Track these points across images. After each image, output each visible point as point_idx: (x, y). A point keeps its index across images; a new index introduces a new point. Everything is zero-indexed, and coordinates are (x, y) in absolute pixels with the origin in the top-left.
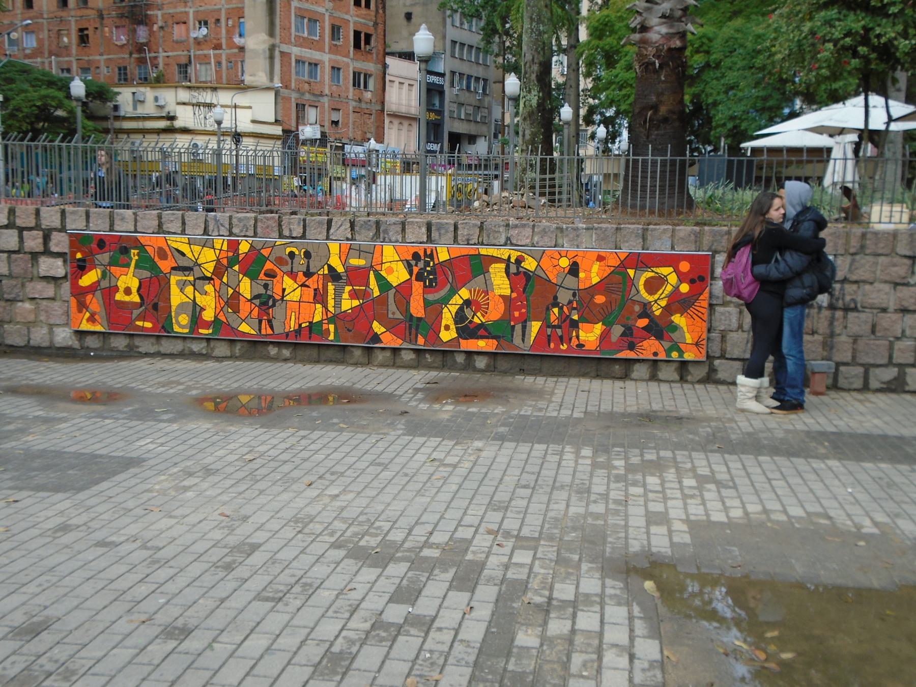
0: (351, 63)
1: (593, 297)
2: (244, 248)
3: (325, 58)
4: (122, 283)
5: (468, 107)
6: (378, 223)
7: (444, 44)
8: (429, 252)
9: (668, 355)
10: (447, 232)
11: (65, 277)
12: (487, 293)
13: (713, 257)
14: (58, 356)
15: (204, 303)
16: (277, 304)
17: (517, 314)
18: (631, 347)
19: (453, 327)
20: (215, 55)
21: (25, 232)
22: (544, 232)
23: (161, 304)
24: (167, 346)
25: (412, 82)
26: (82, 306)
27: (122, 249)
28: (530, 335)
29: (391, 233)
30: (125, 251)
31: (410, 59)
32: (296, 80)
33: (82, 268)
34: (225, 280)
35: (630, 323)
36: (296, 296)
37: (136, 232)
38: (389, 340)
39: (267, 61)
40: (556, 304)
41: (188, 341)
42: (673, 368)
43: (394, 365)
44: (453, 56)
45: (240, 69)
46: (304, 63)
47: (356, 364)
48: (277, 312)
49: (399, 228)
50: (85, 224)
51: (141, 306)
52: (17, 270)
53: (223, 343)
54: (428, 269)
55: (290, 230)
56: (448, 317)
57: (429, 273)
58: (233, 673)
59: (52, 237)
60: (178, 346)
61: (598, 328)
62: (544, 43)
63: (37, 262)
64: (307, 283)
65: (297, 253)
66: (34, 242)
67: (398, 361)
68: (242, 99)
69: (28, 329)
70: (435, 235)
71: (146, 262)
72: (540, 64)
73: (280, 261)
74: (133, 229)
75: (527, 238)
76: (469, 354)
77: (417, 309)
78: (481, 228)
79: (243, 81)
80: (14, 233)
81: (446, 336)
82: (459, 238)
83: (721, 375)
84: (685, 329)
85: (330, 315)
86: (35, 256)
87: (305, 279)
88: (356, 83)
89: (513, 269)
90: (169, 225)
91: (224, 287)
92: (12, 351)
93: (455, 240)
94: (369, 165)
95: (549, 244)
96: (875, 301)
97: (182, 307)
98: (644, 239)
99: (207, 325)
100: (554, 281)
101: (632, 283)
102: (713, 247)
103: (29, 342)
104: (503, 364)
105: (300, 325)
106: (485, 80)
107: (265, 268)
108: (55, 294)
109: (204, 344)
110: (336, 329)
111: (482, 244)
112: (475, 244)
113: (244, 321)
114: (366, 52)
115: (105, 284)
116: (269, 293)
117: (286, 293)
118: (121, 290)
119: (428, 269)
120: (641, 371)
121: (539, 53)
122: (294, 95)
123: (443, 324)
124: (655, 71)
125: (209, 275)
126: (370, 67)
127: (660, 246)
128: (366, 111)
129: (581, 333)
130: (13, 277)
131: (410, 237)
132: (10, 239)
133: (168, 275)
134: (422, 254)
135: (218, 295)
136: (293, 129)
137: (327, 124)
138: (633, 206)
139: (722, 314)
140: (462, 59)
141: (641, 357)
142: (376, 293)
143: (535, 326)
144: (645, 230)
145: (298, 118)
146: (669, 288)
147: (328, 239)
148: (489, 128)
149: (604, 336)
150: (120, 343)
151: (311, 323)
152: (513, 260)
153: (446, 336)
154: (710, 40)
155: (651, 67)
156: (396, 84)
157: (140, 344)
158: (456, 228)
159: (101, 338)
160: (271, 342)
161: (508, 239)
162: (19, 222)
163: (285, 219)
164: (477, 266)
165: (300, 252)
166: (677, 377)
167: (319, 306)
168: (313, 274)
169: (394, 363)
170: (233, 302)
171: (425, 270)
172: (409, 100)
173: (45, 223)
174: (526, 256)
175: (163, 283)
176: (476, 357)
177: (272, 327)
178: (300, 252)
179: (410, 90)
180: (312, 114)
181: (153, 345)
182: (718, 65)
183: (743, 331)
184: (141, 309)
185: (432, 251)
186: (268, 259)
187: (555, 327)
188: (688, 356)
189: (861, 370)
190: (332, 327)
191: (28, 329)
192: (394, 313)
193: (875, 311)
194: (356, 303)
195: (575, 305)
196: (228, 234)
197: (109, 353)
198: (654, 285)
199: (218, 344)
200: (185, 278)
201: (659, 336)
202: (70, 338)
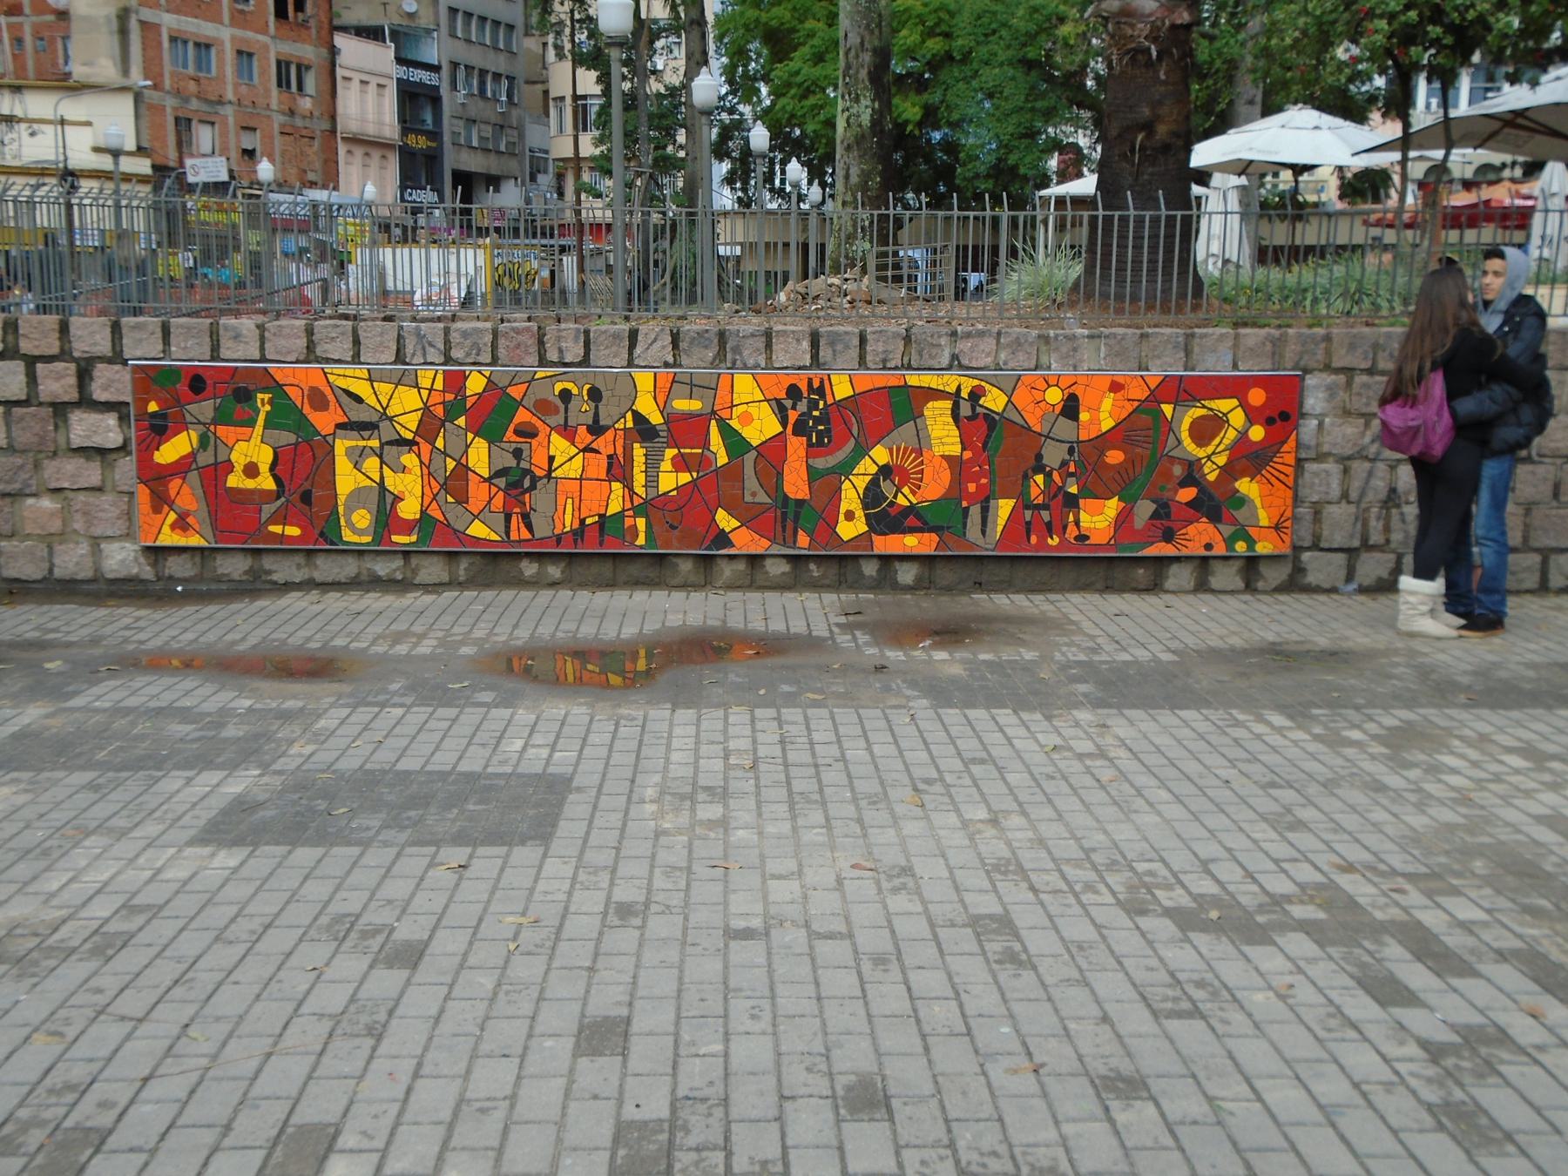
0: (273, 45)
1: (1102, 454)
2: (475, 384)
3: (224, 34)
4: (239, 456)
5: (483, 126)
6: (722, 335)
7: (436, 14)
8: (816, 384)
9: (1230, 547)
10: (847, 347)
11: (123, 448)
12: (920, 453)
13: (1302, 378)
14: (112, 595)
15: (401, 488)
16: (539, 485)
17: (972, 487)
18: (1168, 537)
19: (860, 514)
20: (10, 26)
21: (39, 366)
22: (1017, 344)
23: (316, 493)
24: (326, 568)
25: (382, 81)
26: (161, 501)
27: (236, 393)
28: (995, 522)
29: (746, 353)
30: (244, 396)
31: (376, 39)
32: (172, 74)
33: (160, 429)
34: (440, 443)
35: (1167, 495)
36: (574, 469)
37: (263, 359)
38: (746, 541)
39: (116, 38)
40: (1039, 468)
41: (367, 558)
42: (1235, 569)
43: (752, 585)
44: (453, 35)
45: (60, 53)
46: (185, 42)
47: (684, 586)
48: (539, 500)
49: (760, 343)
50: (160, 347)
51: (278, 498)
52: (23, 437)
53: (435, 559)
54: (816, 413)
55: (561, 351)
56: (850, 498)
57: (817, 421)
58: (416, 1148)
59: (96, 373)
60: (350, 568)
61: (1112, 506)
62: (880, 15)
63: (66, 421)
64: (594, 446)
65: (575, 391)
66: (57, 383)
67: (760, 579)
68: (73, 108)
69: (50, 547)
70: (825, 353)
71: (286, 415)
72: (875, 51)
73: (543, 407)
74: (257, 356)
75: (988, 355)
76: (886, 560)
77: (796, 484)
78: (907, 339)
79: (68, 75)
80: (18, 367)
81: (848, 530)
82: (869, 358)
83: (1311, 578)
84: (1258, 502)
85: (637, 501)
86: (60, 410)
87: (590, 438)
88: (283, 82)
89: (965, 410)
90: (327, 346)
91: (438, 458)
92: (14, 591)
93: (862, 362)
94: (317, 229)
95: (1026, 365)
96: (1561, 445)
97: (357, 496)
98: (1188, 352)
99: (407, 527)
100: (1037, 429)
101: (1169, 427)
102: (1302, 363)
103: (51, 571)
104: (945, 575)
105: (582, 521)
106: (511, 79)
107: (516, 420)
108: (103, 481)
109: (399, 562)
110: (649, 526)
111: (909, 368)
112: (896, 368)
113: (476, 517)
114: (298, 24)
115: (205, 459)
116: (524, 465)
117: (555, 465)
118: (239, 468)
119: (816, 413)
120: (1180, 576)
121: (872, 32)
122: (170, 102)
123: (843, 509)
124: (1150, 64)
125: (409, 436)
126: (307, 51)
127: (1215, 365)
128: (304, 133)
129: (1083, 516)
130: (15, 451)
131: (780, 358)
132: (6, 379)
133: (330, 439)
134: (804, 388)
135: (428, 470)
136: (172, 164)
137: (234, 154)
138: (1105, 296)
139: (1316, 474)
140: (468, 41)
141: (1185, 552)
142: (722, 459)
143: (1004, 508)
144: (1190, 337)
145: (179, 144)
146: (1231, 435)
147: (630, 364)
148: (521, 163)
149: (1123, 519)
150: (234, 567)
151: (602, 516)
152: (965, 394)
153: (848, 530)
154: (952, 14)
155: (1140, 57)
156: (355, 84)
157: (274, 567)
158: (863, 340)
159: (198, 559)
160: (528, 555)
161: (954, 357)
162: (25, 346)
163: (551, 328)
164: (903, 406)
165: (581, 389)
166: (1241, 585)
167: (616, 486)
168: (606, 428)
169: (752, 582)
170: (457, 483)
171: (813, 418)
172: (380, 112)
173: (80, 347)
174: (987, 387)
175: (319, 453)
176: (897, 565)
177: (530, 527)
178: (581, 389)
179: (380, 95)
180: (204, 137)
181: (299, 567)
182: (966, 58)
183: (1349, 502)
184: (279, 503)
185: (822, 382)
186: (520, 403)
187: (1038, 507)
188: (1263, 548)
189: (1537, 558)
190: (641, 523)
191: (50, 547)
192: (754, 494)
193: (1559, 461)
194: (685, 478)
195: (1072, 470)
196: (442, 359)
197: (214, 587)
198: (1205, 430)
199: (425, 561)
200: (363, 443)
201: (1215, 516)
202: (136, 559)
